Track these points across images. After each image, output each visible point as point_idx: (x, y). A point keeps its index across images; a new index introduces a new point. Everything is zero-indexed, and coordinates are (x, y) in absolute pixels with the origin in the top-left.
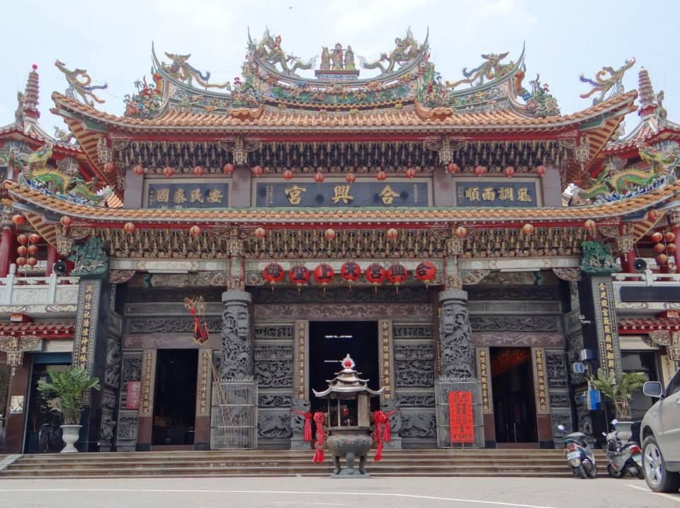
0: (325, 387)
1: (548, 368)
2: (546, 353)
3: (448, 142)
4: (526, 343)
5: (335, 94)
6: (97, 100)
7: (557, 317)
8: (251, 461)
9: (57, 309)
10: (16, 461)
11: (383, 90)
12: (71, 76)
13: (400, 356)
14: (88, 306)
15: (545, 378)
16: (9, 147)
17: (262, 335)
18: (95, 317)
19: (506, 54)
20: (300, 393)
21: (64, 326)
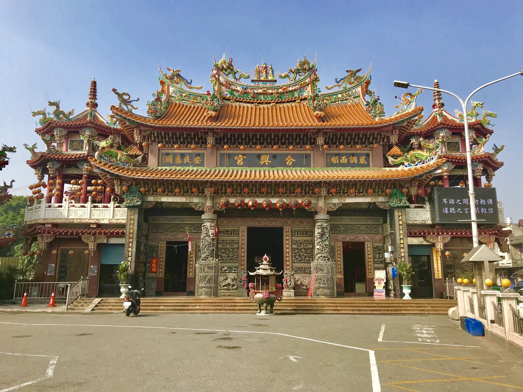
0: (255, 270)
1: (373, 253)
2: (373, 245)
3: (322, 133)
4: (362, 240)
5: (263, 94)
6: (134, 108)
7: (380, 226)
8: (217, 304)
9: (114, 221)
10: (99, 303)
11: (290, 91)
12: (120, 96)
13: (294, 246)
14: (132, 222)
15: (372, 258)
16: (85, 131)
17: (222, 234)
18: (136, 228)
19: (360, 70)
20: (242, 265)
21: (116, 230)
